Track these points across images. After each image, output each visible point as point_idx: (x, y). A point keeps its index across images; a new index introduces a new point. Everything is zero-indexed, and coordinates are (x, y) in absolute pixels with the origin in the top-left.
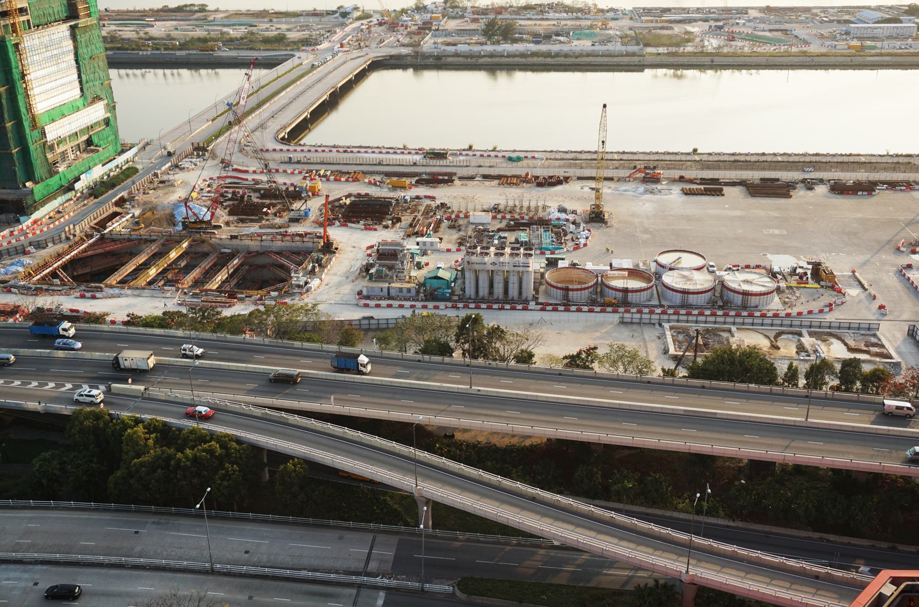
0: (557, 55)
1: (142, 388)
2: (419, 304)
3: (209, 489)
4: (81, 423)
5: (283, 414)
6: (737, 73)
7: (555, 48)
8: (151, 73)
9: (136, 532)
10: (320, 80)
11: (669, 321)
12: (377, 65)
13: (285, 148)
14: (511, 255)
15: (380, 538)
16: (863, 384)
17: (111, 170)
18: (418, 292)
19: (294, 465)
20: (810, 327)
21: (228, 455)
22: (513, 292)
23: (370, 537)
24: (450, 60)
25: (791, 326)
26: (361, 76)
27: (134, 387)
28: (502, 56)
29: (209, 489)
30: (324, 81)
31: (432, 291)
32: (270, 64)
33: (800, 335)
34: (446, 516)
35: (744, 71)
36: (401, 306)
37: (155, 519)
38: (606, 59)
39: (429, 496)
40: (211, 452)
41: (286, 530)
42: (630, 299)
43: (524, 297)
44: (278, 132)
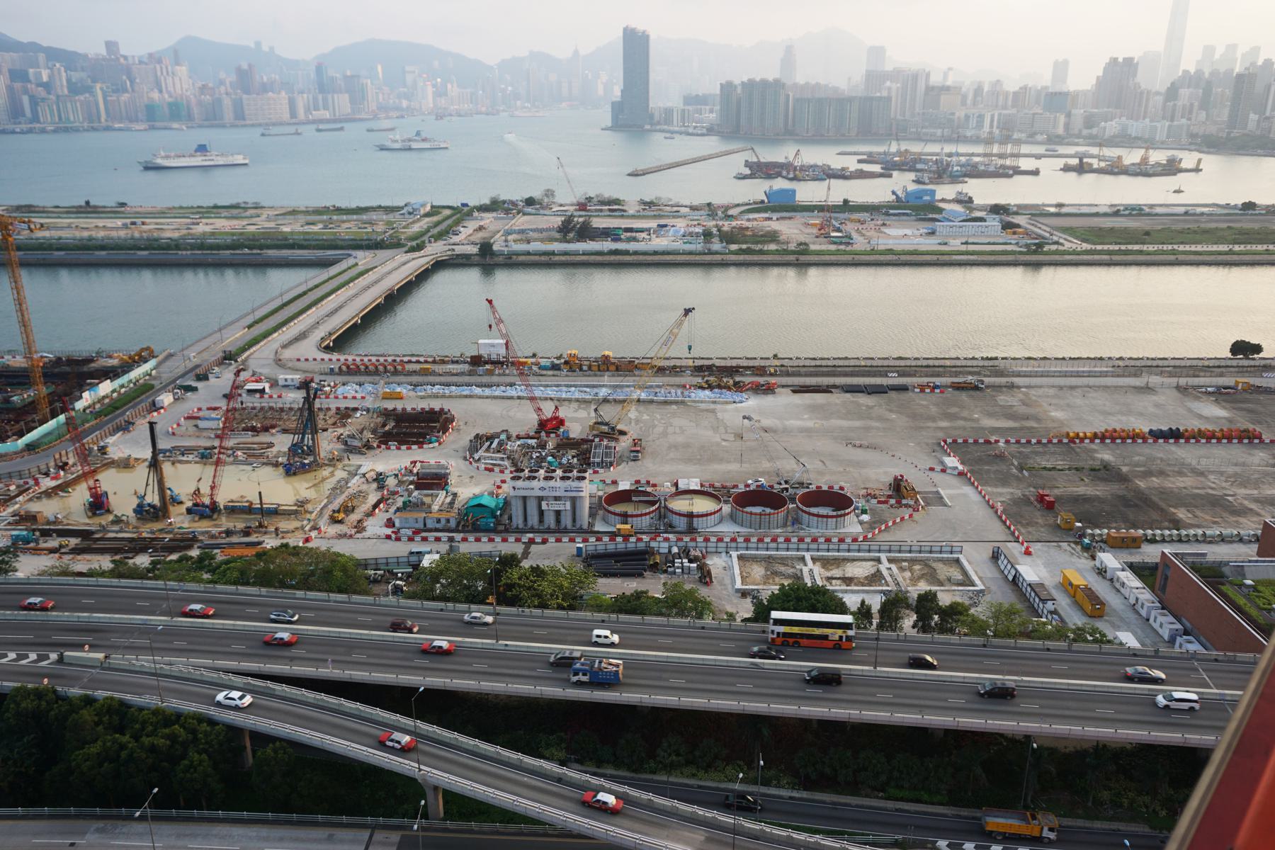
0: (636, 253)
1: (101, 656)
2: (458, 536)
3: (156, 790)
4: (18, 704)
5: (270, 684)
6: (213, 276)
7: (632, 246)
8: (189, 275)
9: (72, 845)
10: (376, 282)
11: (737, 549)
12: (439, 265)
13: (326, 357)
14: (546, 478)
15: (379, 836)
16: (942, 619)
17: (122, 386)
18: (458, 523)
19: (275, 751)
20: (890, 551)
21: (196, 739)
22: (567, 521)
23: (365, 834)
24: (521, 258)
25: (869, 551)
26: (423, 277)
27: (92, 655)
28: (178, 247)
29: (156, 790)
30: (382, 282)
31: (474, 520)
32: (325, 264)
33: (878, 560)
34: (460, 806)
35: (201, 274)
36: (438, 539)
37: (101, 824)
38: (563, 258)
39: (436, 782)
40: (173, 738)
41: (264, 831)
42: (695, 525)
43: (563, 526)
44: (323, 339)
